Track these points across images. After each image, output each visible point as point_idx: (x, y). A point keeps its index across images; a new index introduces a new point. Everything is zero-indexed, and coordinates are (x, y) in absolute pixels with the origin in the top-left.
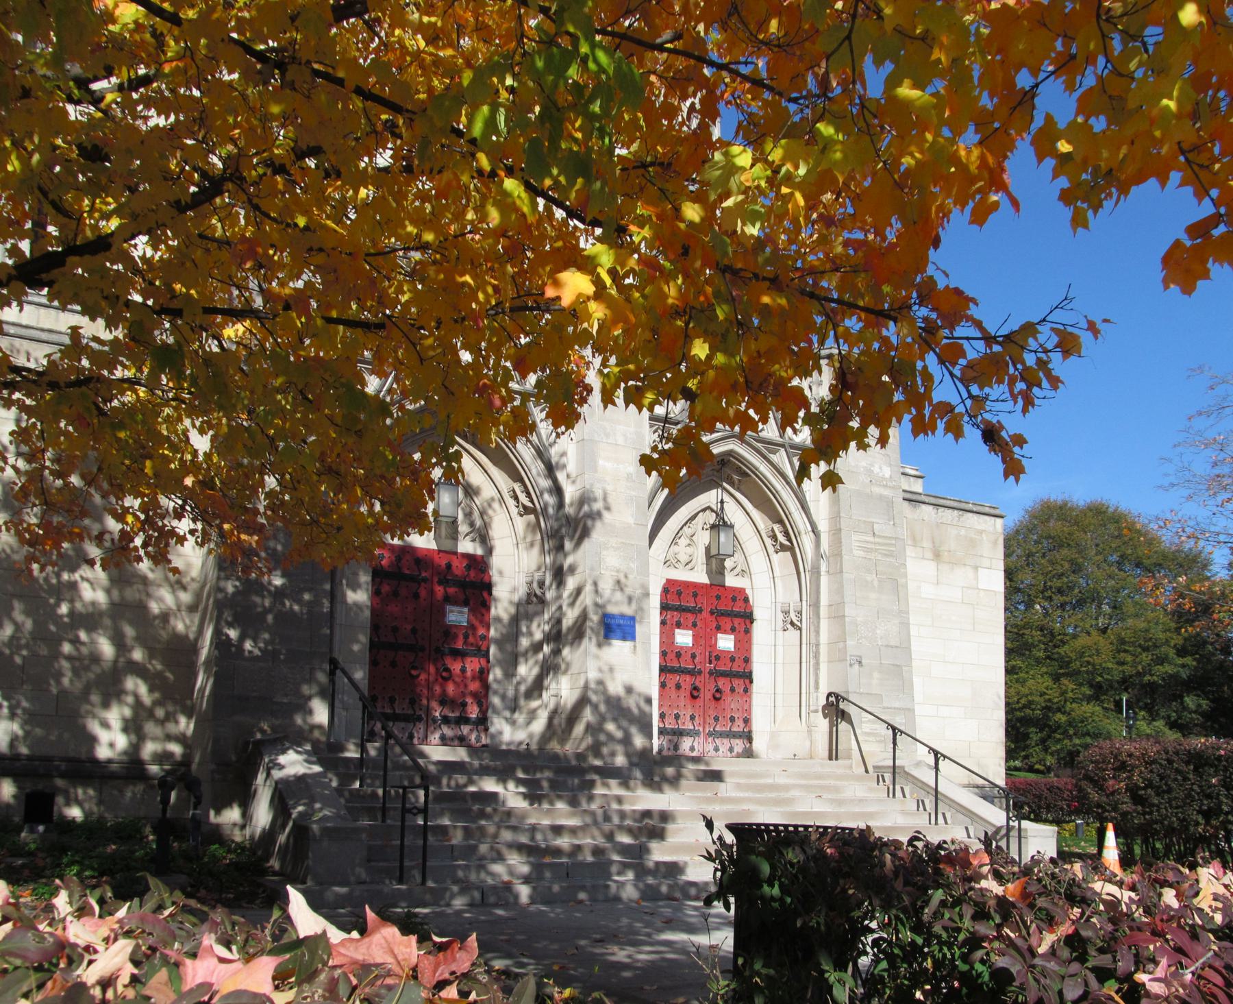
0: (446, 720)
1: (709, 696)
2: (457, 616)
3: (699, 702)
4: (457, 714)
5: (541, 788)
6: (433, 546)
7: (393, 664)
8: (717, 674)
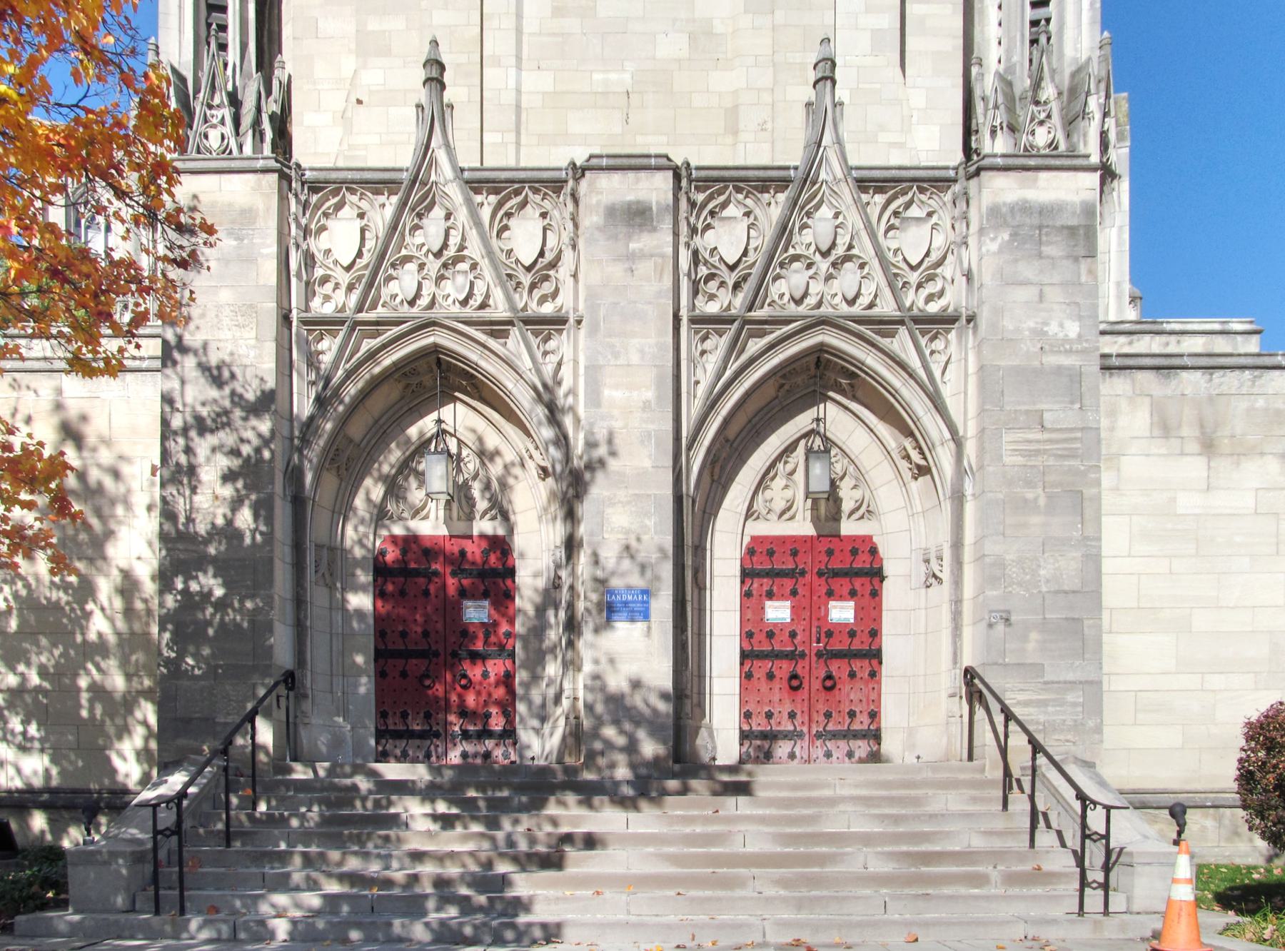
0: (466, 735)
1: (817, 685)
2: (476, 613)
3: (803, 694)
4: (479, 727)
5: (478, 809)
6: (443, 531)
7: (404, 674)
8: (828, 655)
